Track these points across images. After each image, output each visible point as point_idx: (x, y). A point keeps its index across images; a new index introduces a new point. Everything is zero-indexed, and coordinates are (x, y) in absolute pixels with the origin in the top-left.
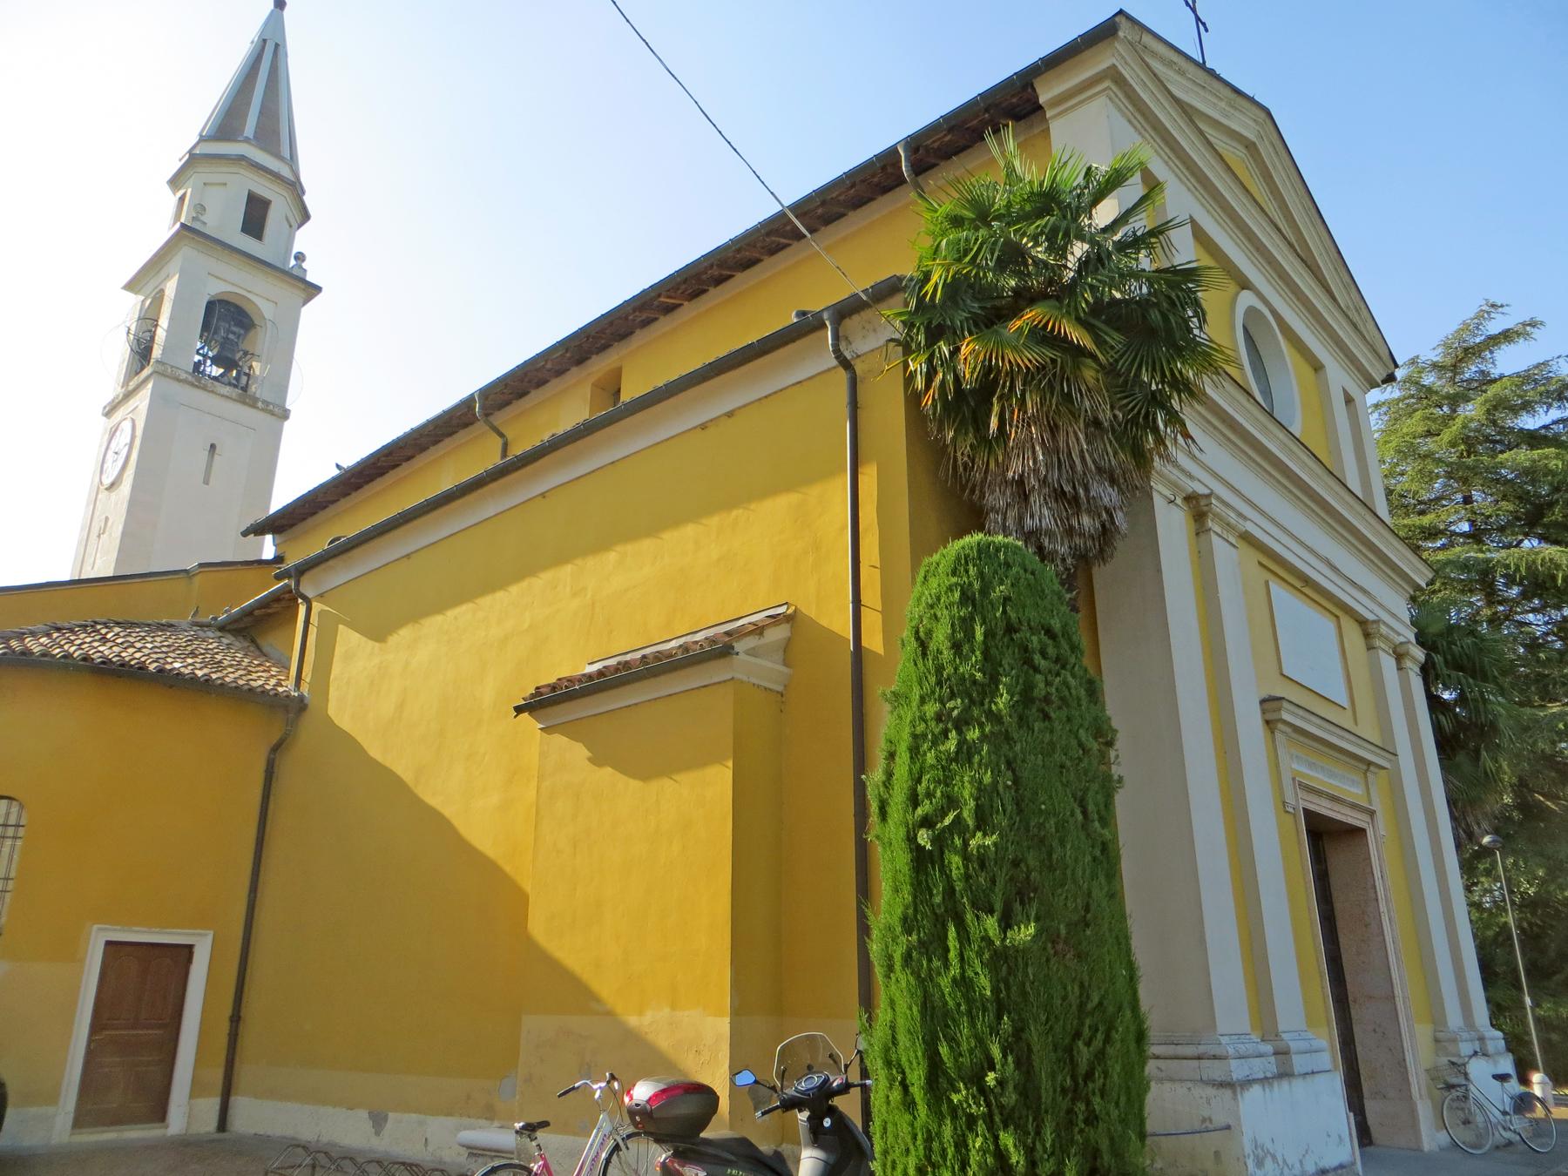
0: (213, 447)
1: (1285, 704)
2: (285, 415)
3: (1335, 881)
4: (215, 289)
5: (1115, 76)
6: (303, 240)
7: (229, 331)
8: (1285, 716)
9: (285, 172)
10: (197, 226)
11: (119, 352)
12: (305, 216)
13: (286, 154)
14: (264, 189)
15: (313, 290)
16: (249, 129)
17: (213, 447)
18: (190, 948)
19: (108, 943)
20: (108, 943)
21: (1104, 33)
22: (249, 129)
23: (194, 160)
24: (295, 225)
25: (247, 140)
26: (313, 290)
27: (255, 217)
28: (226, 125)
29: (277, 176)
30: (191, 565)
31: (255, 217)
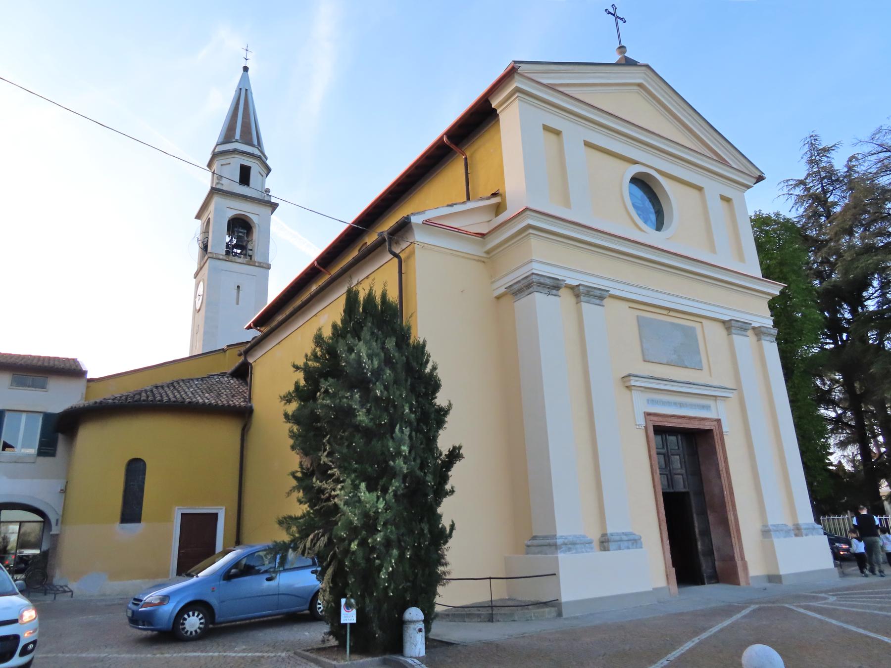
0: (238, 287)
1: (632, 378)
2: (268, 267)
3: (235, 529)
4: (231, 214)
5: (518, 90)
6: (270, 182)
7: (238, 232)
8: (633, 383)
9: (256, 152)
10: (219, 187)
11: (196, 249)
12: (269, 170)
13: (256, 143)
14: (247, 162)
15: (274, 206)
16: (238, 136)
17: (238, 287)
18: (216, 514)
19: (183, 514)
20: (183, 514)
21: (511, 73)
22: (238, 136)
23: (215, 155)
24: (265, 175)
25: (237, 141)
26: (274, 206)
27: (245, 176)
28: (228, 136)
29: (252, 155)
30: (225, 347)
31: (245, 176)
